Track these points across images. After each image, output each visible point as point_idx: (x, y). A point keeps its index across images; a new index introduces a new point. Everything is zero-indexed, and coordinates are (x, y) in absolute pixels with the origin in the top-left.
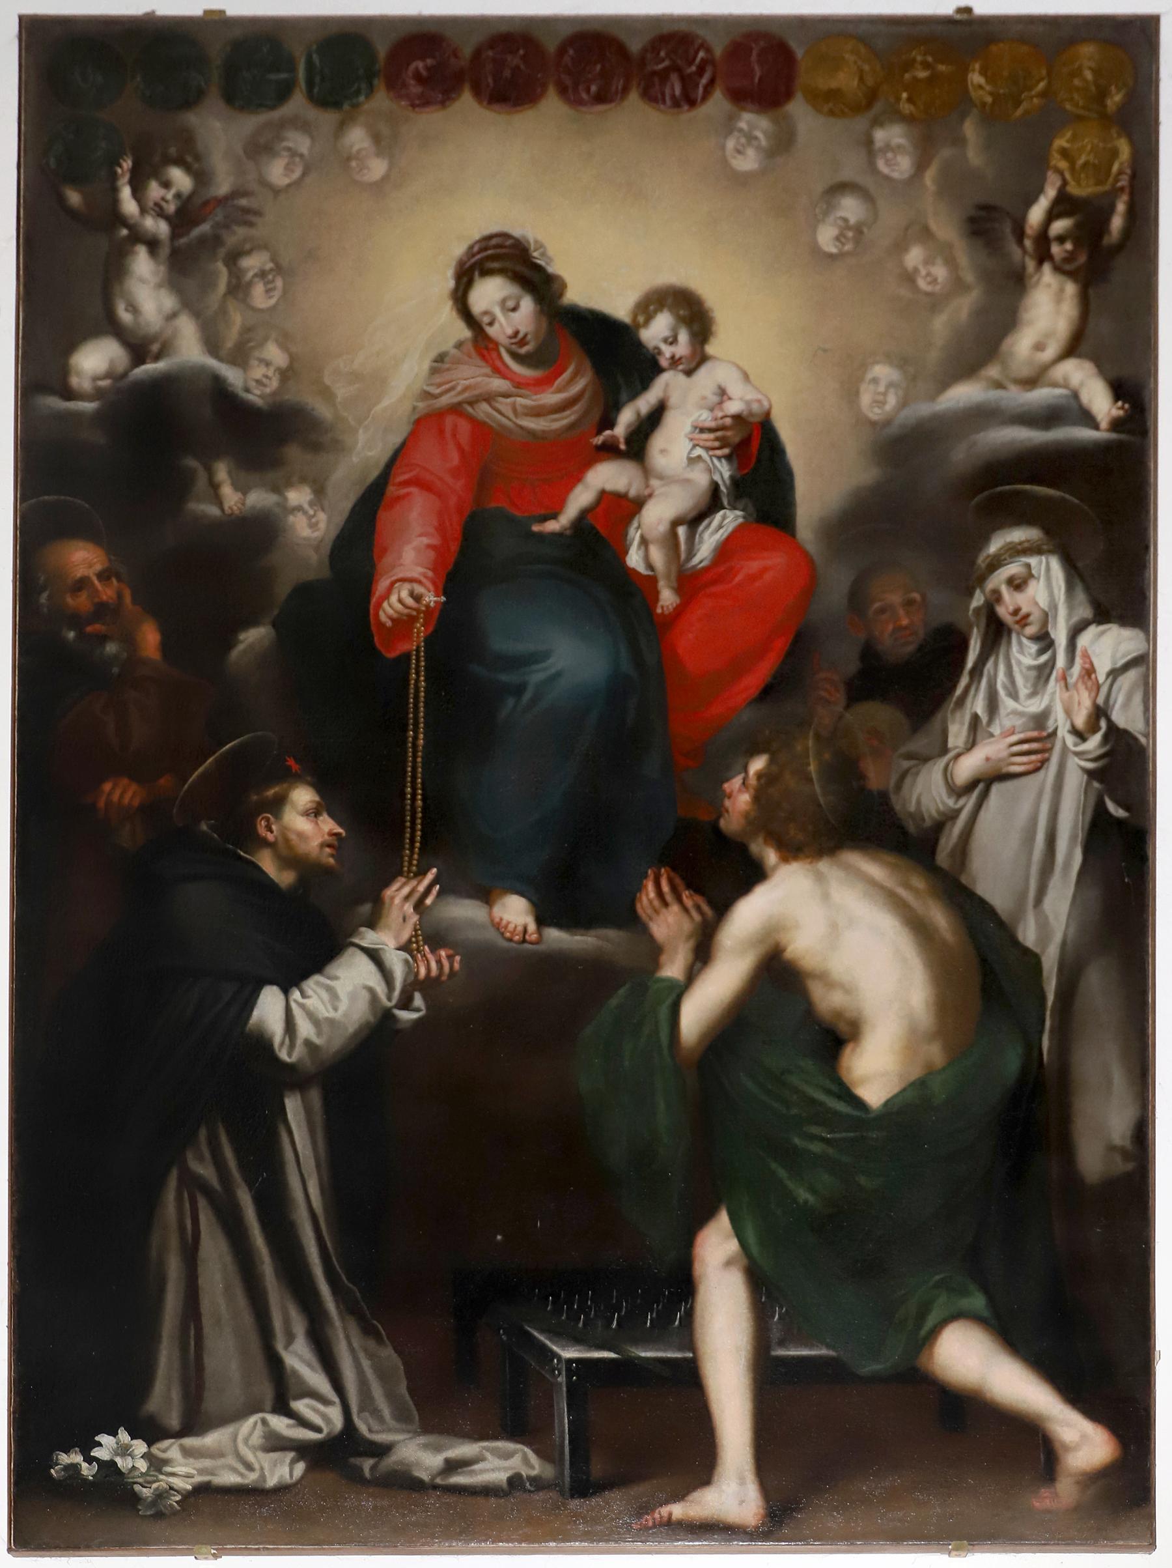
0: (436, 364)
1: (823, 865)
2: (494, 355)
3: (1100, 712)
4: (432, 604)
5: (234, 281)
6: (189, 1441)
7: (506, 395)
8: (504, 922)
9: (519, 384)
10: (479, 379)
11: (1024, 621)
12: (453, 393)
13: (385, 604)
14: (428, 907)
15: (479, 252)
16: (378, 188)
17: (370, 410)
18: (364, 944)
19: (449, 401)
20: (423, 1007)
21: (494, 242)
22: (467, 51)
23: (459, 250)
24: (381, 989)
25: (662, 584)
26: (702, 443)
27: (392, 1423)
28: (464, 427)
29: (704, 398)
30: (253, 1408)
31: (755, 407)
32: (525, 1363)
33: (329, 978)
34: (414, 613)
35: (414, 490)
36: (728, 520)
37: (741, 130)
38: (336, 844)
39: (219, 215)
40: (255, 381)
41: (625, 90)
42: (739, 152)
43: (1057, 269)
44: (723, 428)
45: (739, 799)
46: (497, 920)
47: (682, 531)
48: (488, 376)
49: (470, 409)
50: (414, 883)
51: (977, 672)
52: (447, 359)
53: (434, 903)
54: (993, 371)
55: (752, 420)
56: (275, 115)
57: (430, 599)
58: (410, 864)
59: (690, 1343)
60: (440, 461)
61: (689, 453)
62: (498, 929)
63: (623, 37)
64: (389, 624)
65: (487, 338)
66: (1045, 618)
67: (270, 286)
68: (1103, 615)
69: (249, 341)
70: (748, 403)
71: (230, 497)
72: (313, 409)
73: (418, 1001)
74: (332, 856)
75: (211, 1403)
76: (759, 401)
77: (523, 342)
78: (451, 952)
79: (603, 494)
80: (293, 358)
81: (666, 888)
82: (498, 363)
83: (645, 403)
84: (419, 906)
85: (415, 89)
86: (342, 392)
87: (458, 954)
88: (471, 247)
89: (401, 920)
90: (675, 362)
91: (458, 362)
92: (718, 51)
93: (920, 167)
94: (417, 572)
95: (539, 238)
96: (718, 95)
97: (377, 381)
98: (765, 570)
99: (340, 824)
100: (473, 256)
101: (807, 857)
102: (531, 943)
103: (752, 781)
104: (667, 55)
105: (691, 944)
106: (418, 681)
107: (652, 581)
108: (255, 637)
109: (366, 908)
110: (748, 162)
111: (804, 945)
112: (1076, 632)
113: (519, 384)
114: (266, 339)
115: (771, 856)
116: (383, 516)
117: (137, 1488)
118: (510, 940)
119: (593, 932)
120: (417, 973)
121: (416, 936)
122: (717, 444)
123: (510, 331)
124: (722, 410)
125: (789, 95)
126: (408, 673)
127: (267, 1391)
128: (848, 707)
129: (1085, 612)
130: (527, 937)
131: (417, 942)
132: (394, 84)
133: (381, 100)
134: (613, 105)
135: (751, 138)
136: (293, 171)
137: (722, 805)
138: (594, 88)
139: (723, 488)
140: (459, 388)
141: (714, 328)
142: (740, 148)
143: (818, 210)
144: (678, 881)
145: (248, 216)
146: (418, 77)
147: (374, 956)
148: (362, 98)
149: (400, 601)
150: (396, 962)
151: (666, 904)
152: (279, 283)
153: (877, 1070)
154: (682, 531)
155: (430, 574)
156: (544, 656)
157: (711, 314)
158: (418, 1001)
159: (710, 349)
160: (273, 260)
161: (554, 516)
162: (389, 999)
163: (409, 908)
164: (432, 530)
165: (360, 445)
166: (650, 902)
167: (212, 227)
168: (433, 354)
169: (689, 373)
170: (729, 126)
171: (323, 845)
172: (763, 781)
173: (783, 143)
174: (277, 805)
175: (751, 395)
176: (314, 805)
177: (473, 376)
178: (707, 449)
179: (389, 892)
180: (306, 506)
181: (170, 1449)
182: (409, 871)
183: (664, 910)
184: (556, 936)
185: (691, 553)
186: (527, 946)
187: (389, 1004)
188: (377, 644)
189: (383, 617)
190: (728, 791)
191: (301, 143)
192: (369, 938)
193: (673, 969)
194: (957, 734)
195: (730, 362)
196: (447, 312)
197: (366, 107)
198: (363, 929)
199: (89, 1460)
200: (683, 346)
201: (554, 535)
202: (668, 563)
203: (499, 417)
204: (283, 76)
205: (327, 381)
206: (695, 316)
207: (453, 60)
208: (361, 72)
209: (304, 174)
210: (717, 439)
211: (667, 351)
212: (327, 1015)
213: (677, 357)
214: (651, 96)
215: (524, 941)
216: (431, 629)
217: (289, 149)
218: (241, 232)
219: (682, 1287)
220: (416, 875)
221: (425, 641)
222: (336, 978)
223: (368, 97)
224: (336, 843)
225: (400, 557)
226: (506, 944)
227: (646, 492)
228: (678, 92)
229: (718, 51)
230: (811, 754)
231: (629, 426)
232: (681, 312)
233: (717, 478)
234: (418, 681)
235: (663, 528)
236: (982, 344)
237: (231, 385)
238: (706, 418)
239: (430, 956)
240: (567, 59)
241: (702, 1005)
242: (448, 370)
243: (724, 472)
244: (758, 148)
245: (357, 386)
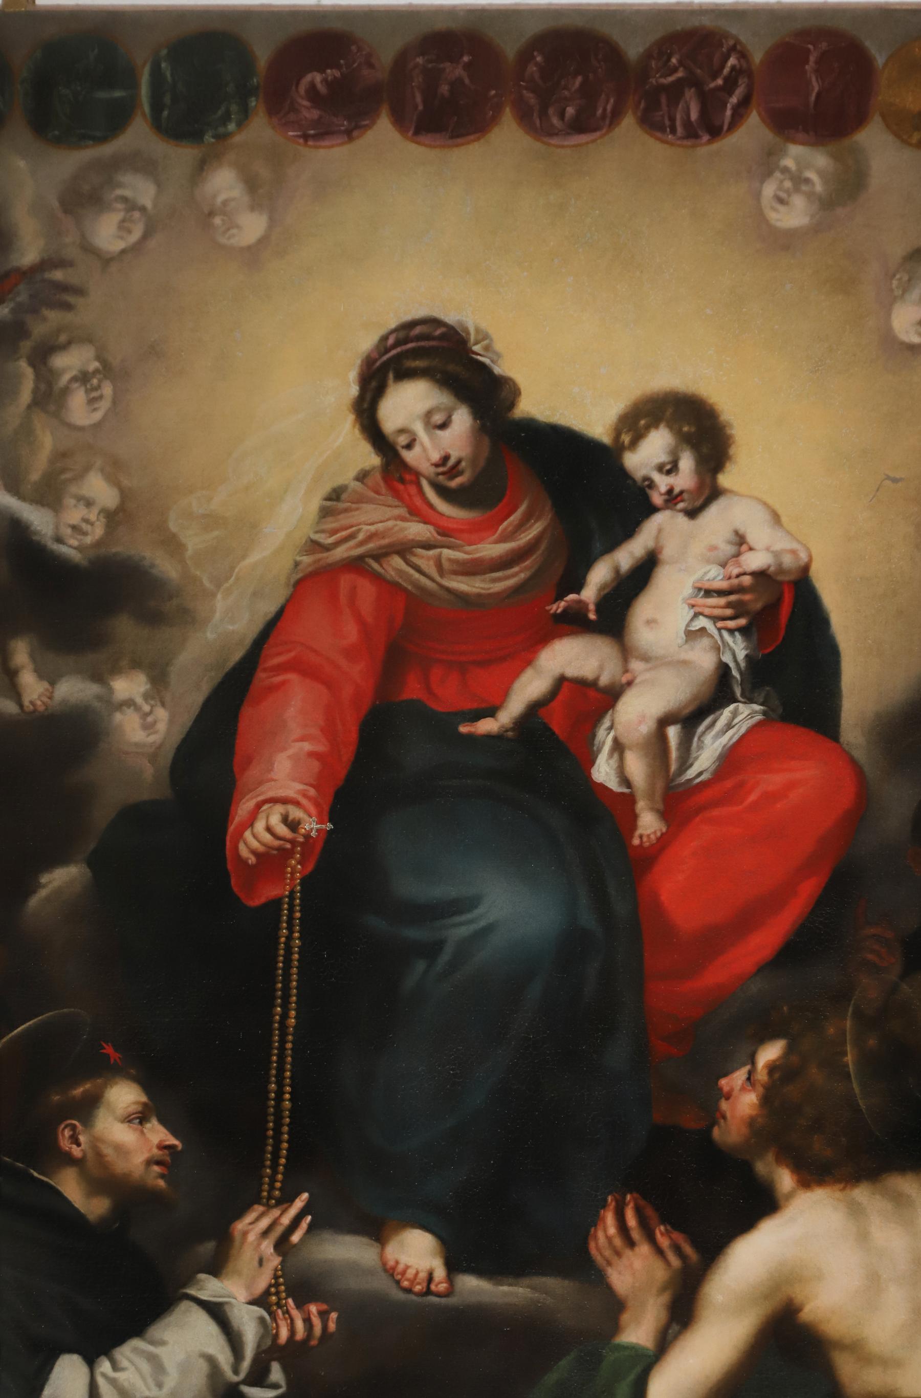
0: (329, 503)
1: (861, 1193)
2: (413, 490)
4: (313, 834)
5: (43, 387)
7: (428, 546)
8: (401, 1267)
9: (444, 532)
10: (390, 523)
12: (352, 543)
13: (248, 834)
14: (295, 1246)
15: (394, 346)
16: (252, 256)
17: (232, 568)
18: (204, 1296)
19: (345, 555)
20: (283, 1382)
21: (418, 330)
22: (386, 56)
23: (367, 342)
24: (224, 1358)
25: (641, 805)
26: (707, 611)
28: (367, 592)
29: (713, 548)
31: (788, 561)
33: (152, 1343)
34: (288, 846)
35: (292, 677)
36: (740, 717)
37: (785, 170)
38: (169, 1160)
39: (23, 295)
40: (70, 527)
41: (616, 116)
42: (781, 201)
44: (740, 590)
45: (741, 1103)
46: (391, 1263)
47: (673, 733)
48: (403, 519)
49: (375, 565)
50: (276, 1212)
52: (344, 496)
53: (302, 1240)
55: (780, 578)
56: (107, 150)
57: (311, 825)
58: (272, 1187)
60: (334, 635)
61: (688, 625)
62: (392, 1275)
63: (615, 34)
64: (252, 860)
65: (404, 465)
67: (94, 394)
69: (64, 470)
70: (777, 554)
71: (33, 687)
72: (153, 566)
73: (276, 1373)
74: (162, 1176)
76: (794, 552)
77: (454, 472)
78: (324, 1307)
79: (562, 681)
80: (125, 494)
81: (631, 1220)
82: (418, 502)
83: (626, 556)
84: (282, 1245)
85: (311, 114)
86: (194, 541)
87: (334, 1310)
88: (384, 338)
89: (256, 1263)
90: (672, 498)
91: (360, 500)
92: (757, 57)
94: (292, 789)
95: (484, 325)
96: (754, 119)
97: (247, 527)
98: (791, 786)
99: (175, 1133)
100: (387, 351)
101: (837, 1181)
102: (438, 1295)
103: (762, 1075)
104: (681, 63)
105: (665, 1298)
106: (291, 938)
107: (626, 802)
108: (62, 879)
109: (208, 1247)
110: (794, 215)
111: (829, 1302)
114: (87, 469)
115: (785, 1180)
116: (248, 713)
118: (408, 1291)
119: (526, 1281)
120: (276, 1336)
121: (277, 1285)
122: (729, 612)
123: (436, 456)
124: (739, 565)
125: (860, 120)
126: (278, 928)
128: (905, 974)
130: (433, 1287)
131: (277, 1293)
132: (279, 102)
133: (260, 129)
134: (598, 134)
135: (799, 181)
136: (129, 232)
137: (717, 1108)
138: (570, 111)
139: (735, 673)
140: (361, 536)
141: (732, 451)
142: (783, 195)
143: (895, 283)
144: (650, 1212)
145: (62, 296)
146: (313, 94)
147: (216, 1312)
148: (231, 127)
149: (269, 829)
150: (248, 1321)
151: (631, 1243)
152: (107, 390)
154: (673, 733)
155: (312, 792)
156: (472, 903)
157: (729, 431)
158: (276, 1373)
159: (724, 480)
160: (98, 358)
161: (491, 712)
162: (236, 1371)
163: (267, 1247)
164: (315, 731)
165: (218, 615)
166: (609, 1239)
167: (13, 311)
168: (326, 488)
169: (692, 514)
170: (767, 164)
171: (149, 1162)
172: (777, 1076)
173: (849, 186)
174: (87, 1108)
175: (782, 543)
176: (140, 1108)
177: (380, 519)
178: (715, 619)
179: (240, 1226)
180: (139, 700)
182: (270, 1197)
183: (628, 1253)
184: (472, 1285)
185: (685, 762)
186: (433, 1299)
187: (235, 1379)
188: (235, 889)
189: (244, 851)
190: (726, 1089)
191: (141, 189)
192: (210, 1288)
193: (638, 1333)
195: (750, 497)
196: (347, 429)
197: (237, 139)
198: (202, 1276)
200: (685, 477)
201: (489, 737)
202: (652, 777)
203: (417, 575)
204: (118, 94)
205: (173, 527)
206: (703, 432)
207: (365, 72)
208: (231, 88)
209: (146, 236)
210: (729, 605)
211: (663, 482)
212: (147, 1393)
213: (677, 490)
214: (652, 123)
215: (428, 1292)
216: (310, 867)
217: (125, 200)
218: (53, 316)
220: (279, 1202)
221: (301, 884)
222: (163, 1343)
223: (240, 125)
224: (168, 1159)
225: (270, 770)
226: (401, 1296)
227: (624, 680)
228: (694, 116)
229: (757, 57)
230: (848, 1038)
231: (602, 588)
232: (686, 429)
233: (727, 658)
234: (291, 938)
235: (646, 728)
237: (36, 533)
238: (715, 577)
239: (295, 1313)
240: (532, 69)
242: (346, 510)
243: (738, 649)
244: (810, 196)
245: (216, 533)
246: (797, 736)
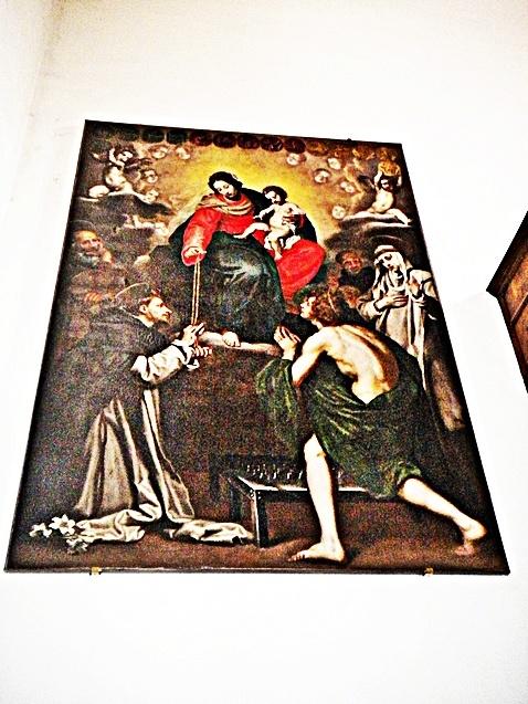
3: (421, 292)
6: (94, 521)
11: (392, 268)
24: (183, 358)
27: (182, 514)
28: (213, 213)
30: (123, 507)
32: (239, 492)
43: (385, 189)
45: (306, 311)
47: (282, 240)
51: (380, 279)
54: (371, 210)
59: (305, 484)
66: (398, 268)
68: (416, 267)
70: (59, 411)
75: (105, 505)
83: (268, 210)
84: (197, 334)
90: (276, 202)
93: (342, 167)
112: (408, 271)
113: (229, 204)
117: (68, 541)
127: (130, 501)
128: (340, 286)
129: (410, 266)
132: (192, 140)
147: (180, 348)
153: (367, 390)
154: (282, 240)
158: (196, 362)
181: (84, 524)
184: (246, 346)
194: (376, 294)
199: (48, 528)
200: (278, 198)
206: (282, 194)
219: (301, 463)
236: (367, 204)
241: (299, 370)
246: (307, 241)
